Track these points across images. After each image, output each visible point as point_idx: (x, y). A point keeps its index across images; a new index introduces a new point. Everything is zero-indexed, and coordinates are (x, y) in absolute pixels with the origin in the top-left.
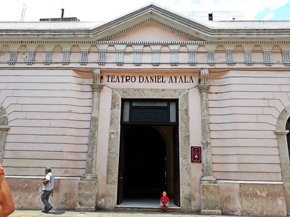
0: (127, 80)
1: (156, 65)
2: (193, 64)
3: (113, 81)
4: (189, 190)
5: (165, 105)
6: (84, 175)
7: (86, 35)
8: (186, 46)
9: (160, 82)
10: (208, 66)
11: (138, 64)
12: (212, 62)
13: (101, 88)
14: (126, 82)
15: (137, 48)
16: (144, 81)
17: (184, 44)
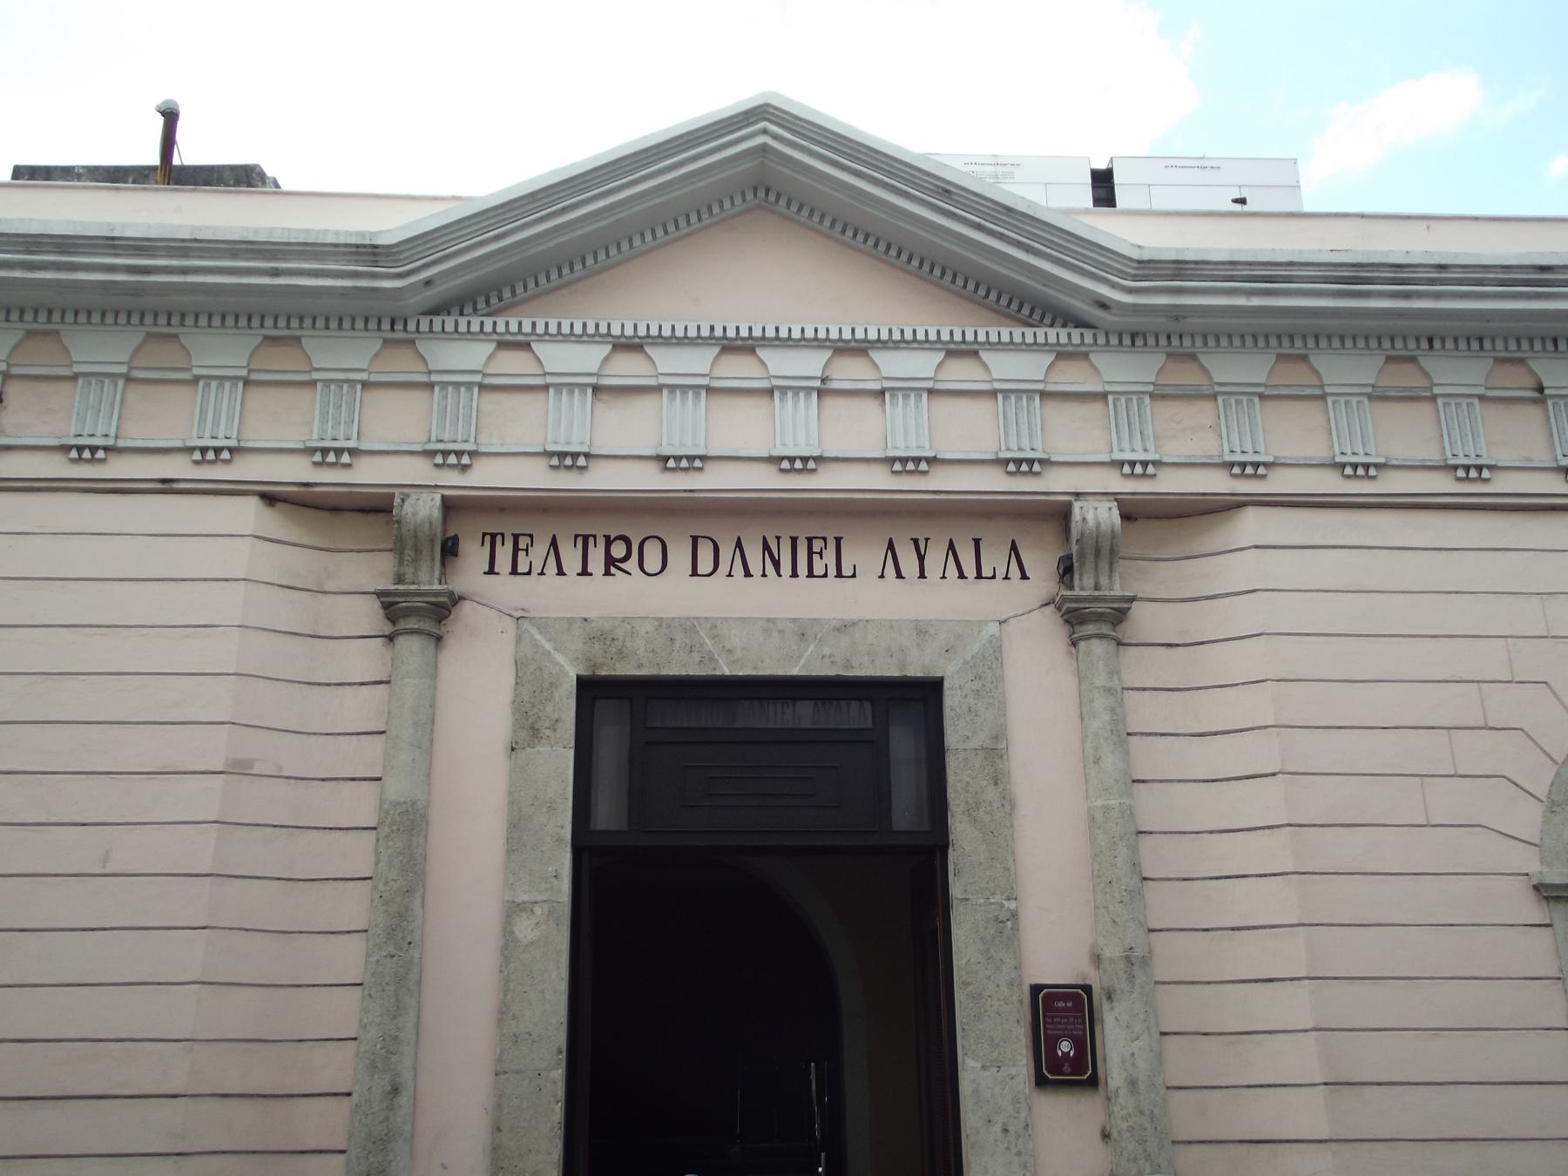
0: (610, 562)
3: (522, 568)
5: (856, 716)
8: (975, 354)
9: (825, 575)
10: (1115, 483)
11: (798, 465)
12: (1140, 456)
13: (442, 610)
14: (607, 573)
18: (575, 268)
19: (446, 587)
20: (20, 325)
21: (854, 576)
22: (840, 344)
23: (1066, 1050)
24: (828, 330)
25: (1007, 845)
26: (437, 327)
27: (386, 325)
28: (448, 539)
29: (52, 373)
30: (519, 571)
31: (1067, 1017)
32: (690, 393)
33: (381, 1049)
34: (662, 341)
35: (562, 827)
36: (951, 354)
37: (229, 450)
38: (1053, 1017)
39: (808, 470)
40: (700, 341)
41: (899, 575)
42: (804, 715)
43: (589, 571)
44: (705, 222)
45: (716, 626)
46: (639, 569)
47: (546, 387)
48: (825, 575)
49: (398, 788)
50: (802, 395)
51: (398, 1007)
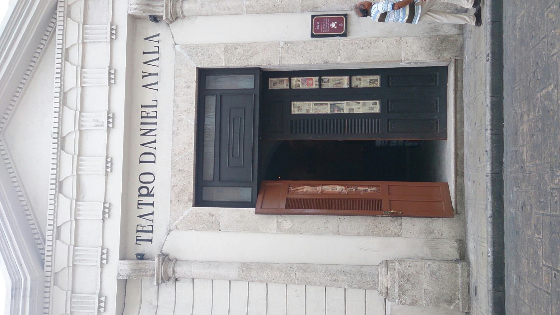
0: (148, 195)
1: (113, 120)
2: (114, 32)
3: (150, 229)
4: (410, 40)
5: (211, 102)
6: (381, 293)
7: (24, 296)
8: (67, 50)
11: (111, 120)
13: (165, 258)
14: (153, 195)
15: (67, 170)
16: (152, 151)
17: (64, 54)
18: (27, 209)
19: (156, 258)
20: (52, 288)
21: (157, 101)
22: (61, 103)
23: (335, 25)
24: (55, 107)
25: (260, 45)
26: (49, 264)
27: (48, 284)
28: (137, 258)
29: (77, 117)
30: (151, 230)
31: (323, 24)
32: (81, 163)
33: (329, 277)
34: (58, 174)
35: (250, 211)
36: (67, 59)
37: (100, 308)
38: (323, 30)
39: (107, 258)
40: (58, 159)
41: (157, 83)
42: (210, 121)
43: (152, 203)
44: (9, 157)
45: (175, 153)
46: (152, 183)
47: (76, 220)
48: (156, 112)
49: (234, 273)
50: (82, 119)
51: (314, 272)
